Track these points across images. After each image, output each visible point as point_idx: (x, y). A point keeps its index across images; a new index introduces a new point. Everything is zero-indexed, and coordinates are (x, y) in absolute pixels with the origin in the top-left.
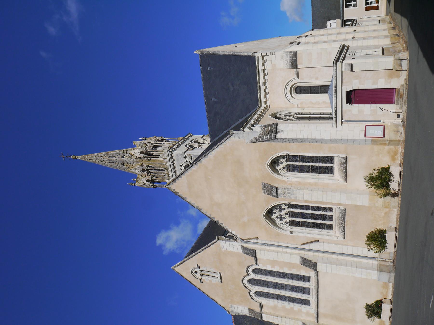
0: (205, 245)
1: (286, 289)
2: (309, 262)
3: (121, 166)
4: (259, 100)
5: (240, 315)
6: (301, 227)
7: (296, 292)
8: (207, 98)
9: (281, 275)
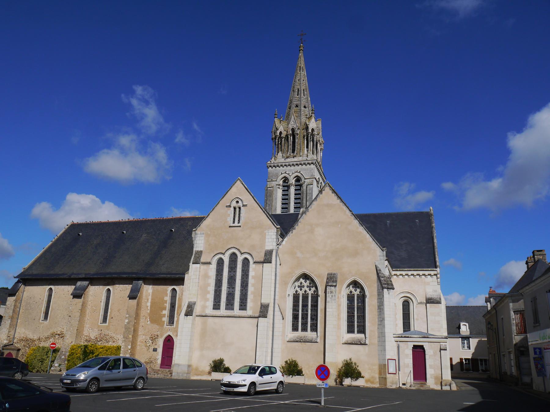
1: (229, 288)
2: (266, 311)
3: (295, 103)
4: (398, 269)
9: (244, 284)
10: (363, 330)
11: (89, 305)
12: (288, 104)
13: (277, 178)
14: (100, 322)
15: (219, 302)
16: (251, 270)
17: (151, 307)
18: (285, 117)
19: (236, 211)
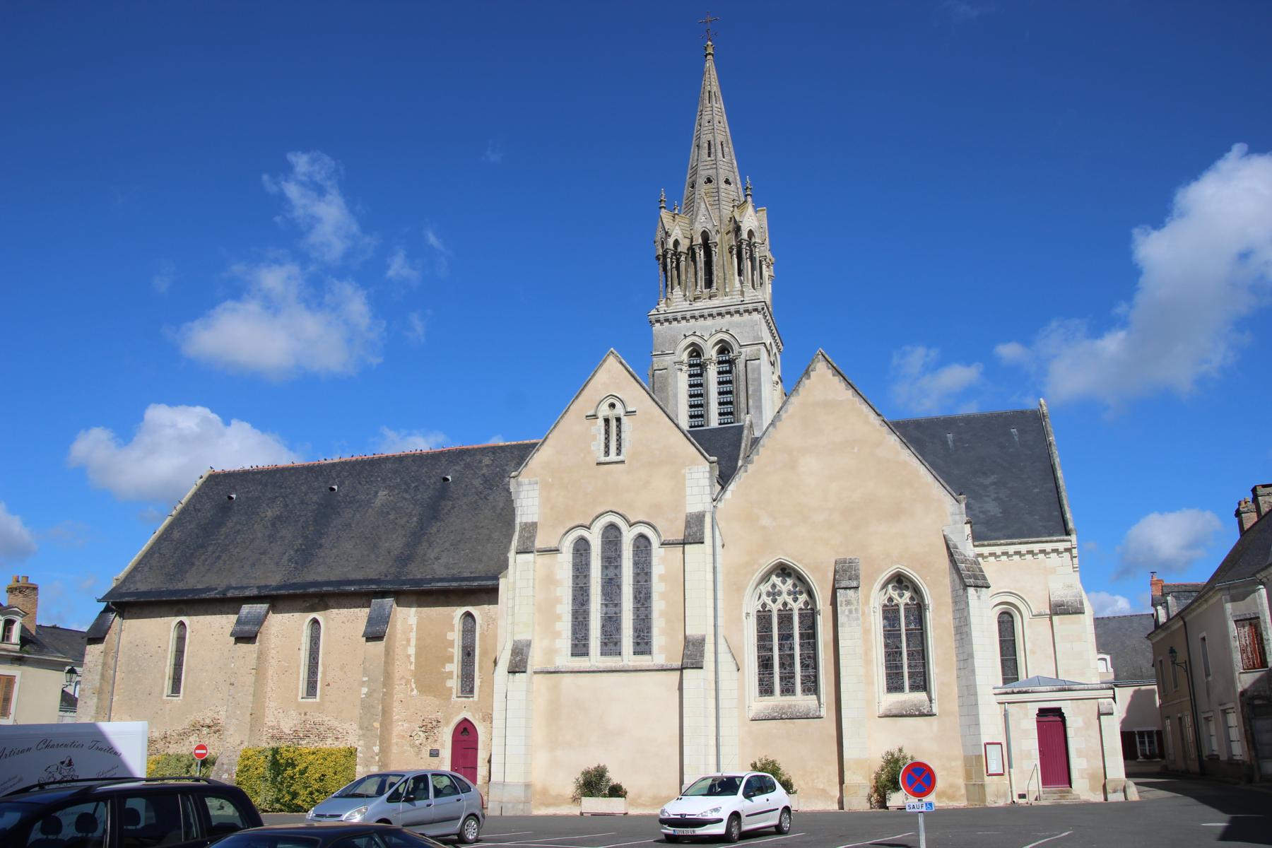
1: (606, 605)
2: (699, 654)
4: (986, 543)
6: (758, 635)
7: (603, 626)
10: (922, 683)
11: (273, 658)
14: (300, 696)
15: (585, 639)
16: (655, 560)
17: (418, 655)
18: (683, 205)
19: (611, 428)
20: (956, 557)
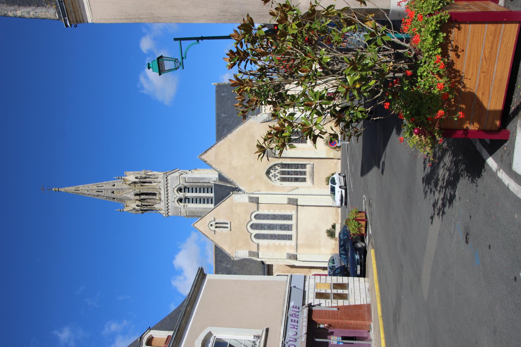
0: (221, 201)
1: (276, 229)
5: (241, 259)
7: (283, 230)
8: (218, 115)
12: (110, 200)
13: (178, 208)
20: (267, 120)
